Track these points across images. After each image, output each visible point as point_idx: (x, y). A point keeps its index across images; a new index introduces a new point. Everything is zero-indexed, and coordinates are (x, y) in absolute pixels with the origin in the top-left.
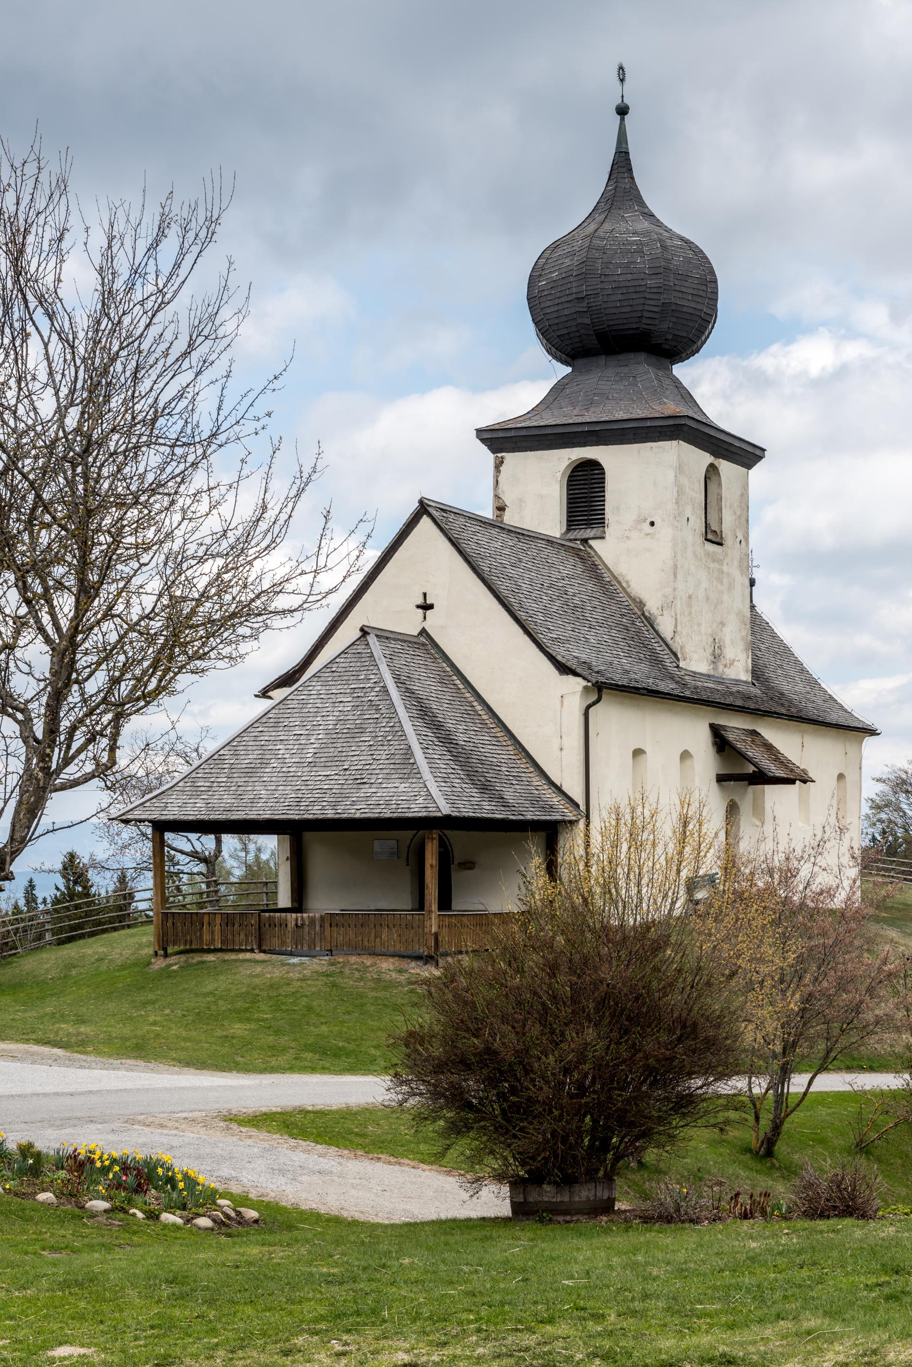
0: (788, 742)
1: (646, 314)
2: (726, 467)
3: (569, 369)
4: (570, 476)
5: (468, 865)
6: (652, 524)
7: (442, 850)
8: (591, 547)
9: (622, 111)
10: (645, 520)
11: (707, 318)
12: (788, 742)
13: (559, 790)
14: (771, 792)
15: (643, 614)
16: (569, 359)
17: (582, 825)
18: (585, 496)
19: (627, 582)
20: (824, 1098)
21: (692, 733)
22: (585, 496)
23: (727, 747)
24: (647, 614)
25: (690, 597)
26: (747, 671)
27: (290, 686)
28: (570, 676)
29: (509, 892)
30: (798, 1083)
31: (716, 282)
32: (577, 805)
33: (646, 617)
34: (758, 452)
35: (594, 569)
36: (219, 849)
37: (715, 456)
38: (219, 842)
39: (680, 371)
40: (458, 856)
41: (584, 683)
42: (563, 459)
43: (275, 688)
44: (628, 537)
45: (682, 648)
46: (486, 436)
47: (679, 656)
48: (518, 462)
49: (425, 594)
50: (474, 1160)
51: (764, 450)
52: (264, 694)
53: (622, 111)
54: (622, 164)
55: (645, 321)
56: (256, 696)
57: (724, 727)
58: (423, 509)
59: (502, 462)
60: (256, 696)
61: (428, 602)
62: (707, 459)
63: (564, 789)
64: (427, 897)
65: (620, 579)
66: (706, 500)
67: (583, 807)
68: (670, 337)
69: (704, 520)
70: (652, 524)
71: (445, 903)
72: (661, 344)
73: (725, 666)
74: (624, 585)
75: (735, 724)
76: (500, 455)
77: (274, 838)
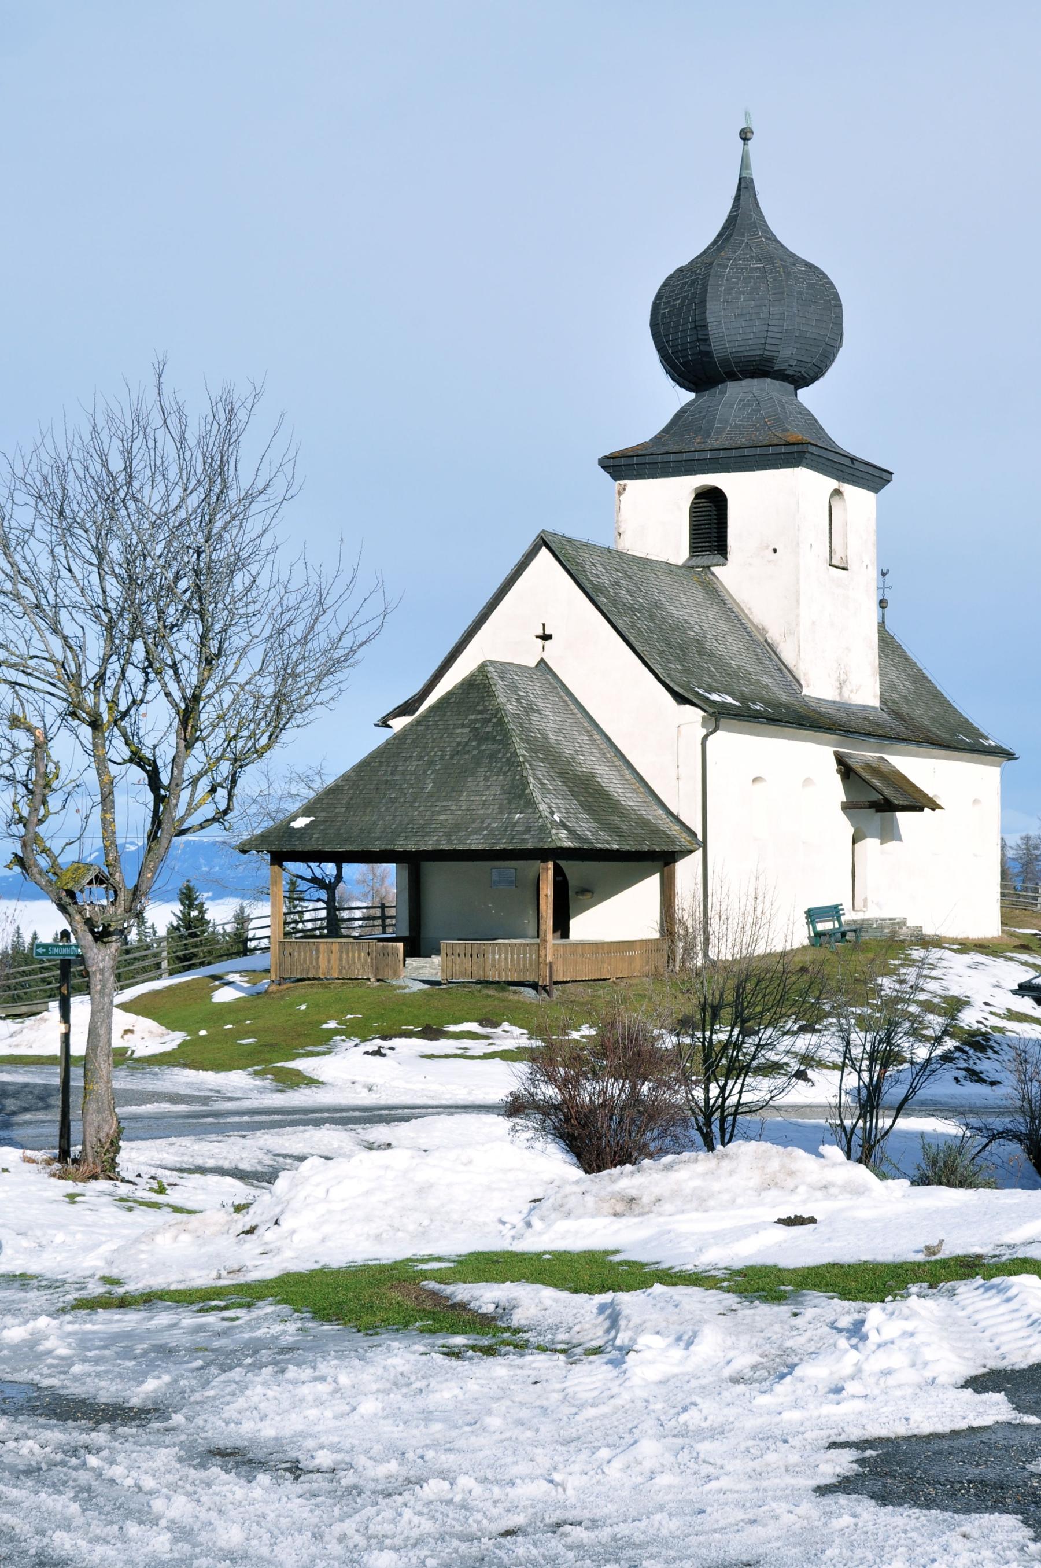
0: (917, 768)
1: (769, 341)
2: (625, 1299)
3: (692, 396)
4: (692, 503)
5: (584, 891)
6: (775, 551)
7: (559, 879)
8: (713, 574)
9: (745, 135)
10: (767, 547)
11: (832, 342)
12: (917, 768)
13: (676, 819)
14: (901, 816)
15: (766, 641)
16: (692, 386)
17: (699, 853)
18: (710, 523)
19: (749, 609)
20: (907, 1135)
21: (814, 760)
22: (710, 523)
23: (852, 774)
24: (769, 640)
25: (814, 623)
26: (875, 696)
27: (412, 715)
28: (688, 706)
29: (622, 917)
30: (884, 1123)
31: (841, 306)
32: (695, 835)
33: (769, 645)
34: (885, 475)
35: (714, 592)
36: (339, 877)
37: (839, 480)
38: (339, 870)
39: (806, 396)
40: (573, 882)
41: (702, 713)
42: (683, 489)
43: (395, 717)
44: (750, 564)
45: (805, 675)
46: (611, 462)
47: (802, 682)
48: (641, 492)
49: (544, 625)
50: (880, 928)
51: (891, 473)
52: (384, 723)
53: (745, 135)
54: (745, 187)
55: (768, 347)
56: (376, 725)
57: (849, 756)
58: (543, 542)
59: (624, 489)
60: (376, 725)
61: (547, 633)
62: (833, 484)
63: (682, 818)
64: (542, 927)
65: (743, 606)
66: (830, 524)
67: (700, 837)
68: (794, 363)
69: (828, 545)
70: (775, 551)
71: (562, 927)
72: (785, 370)
73: (852, 691)
74: (746, 611)
75: (863, 754)
76: (622, 482)
77: (392, 866)
